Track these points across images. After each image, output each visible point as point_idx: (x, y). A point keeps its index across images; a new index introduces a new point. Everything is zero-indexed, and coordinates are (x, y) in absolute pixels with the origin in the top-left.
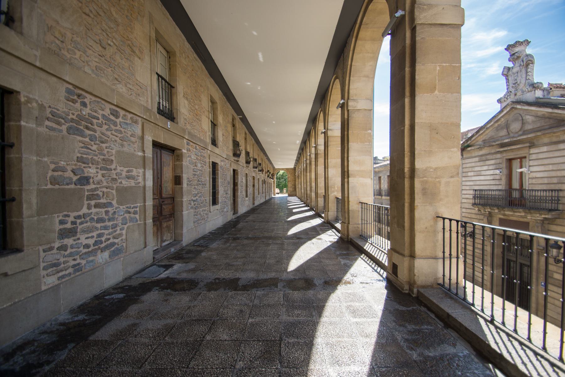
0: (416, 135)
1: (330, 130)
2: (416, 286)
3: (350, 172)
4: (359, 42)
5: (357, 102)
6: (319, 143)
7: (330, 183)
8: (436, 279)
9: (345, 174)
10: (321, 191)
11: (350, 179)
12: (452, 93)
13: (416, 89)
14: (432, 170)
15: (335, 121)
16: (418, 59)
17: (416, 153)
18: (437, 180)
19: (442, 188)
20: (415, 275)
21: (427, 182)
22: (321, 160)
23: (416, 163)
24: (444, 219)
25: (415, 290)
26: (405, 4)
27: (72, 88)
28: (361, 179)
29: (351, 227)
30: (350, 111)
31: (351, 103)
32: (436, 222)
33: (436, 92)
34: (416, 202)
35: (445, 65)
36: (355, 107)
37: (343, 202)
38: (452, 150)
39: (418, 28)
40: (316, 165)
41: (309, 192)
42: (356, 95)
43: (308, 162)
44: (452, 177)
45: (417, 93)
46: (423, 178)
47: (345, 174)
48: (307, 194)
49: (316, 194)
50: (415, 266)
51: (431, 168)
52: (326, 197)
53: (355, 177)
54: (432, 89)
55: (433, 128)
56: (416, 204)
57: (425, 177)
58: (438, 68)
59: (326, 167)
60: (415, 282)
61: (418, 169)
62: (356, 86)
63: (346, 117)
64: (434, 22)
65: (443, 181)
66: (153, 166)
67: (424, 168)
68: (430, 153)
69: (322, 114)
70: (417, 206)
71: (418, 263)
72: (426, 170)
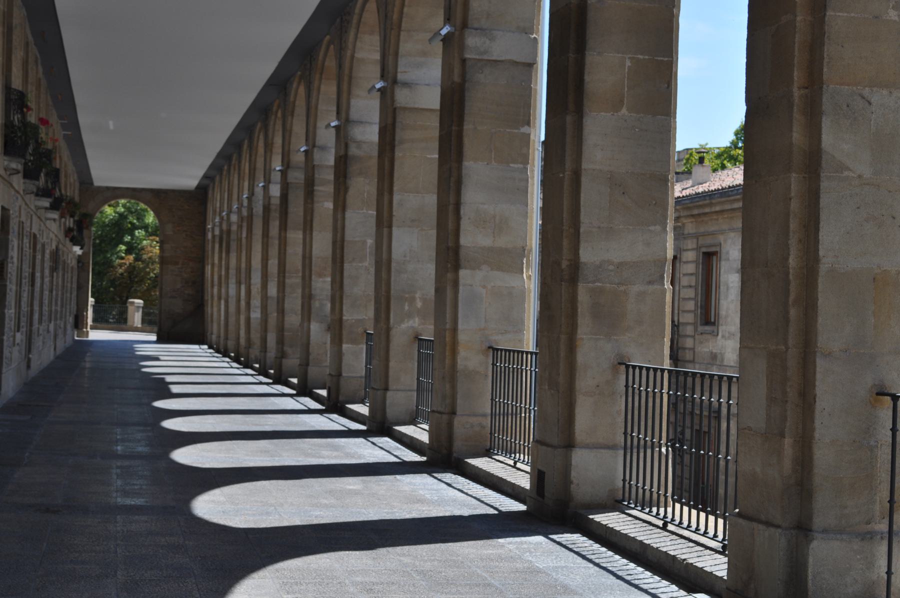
0: (582, 195)
1: (406, 84)
3: (462, 253)
5: (492, 39)
6: (354, 115)
7: (398, 283)
9: (450, 257)
10: (360, 314)
11: (462, 273)
13: (585, 101)
14: (611, 267)
15: (424, 54)
17: (582, 230)
18: (622, 288)
20: (571, 482)
22: (363, 186)
23: (581, 252)
24: (627, 367)
27: (448, 326)
29: (457, 421)
31: (472, 41)
33: (624, 111)
34: (579, 331)
35: (641, 57)
36: (485, 52)
38: (652, 228)
40: (341, 206)
41: (293, 320)
43: (297, 177)
44: (650, 283)
45: (586, 109)
46: (594, 282)
47: (450, 257)
48: (281, 329)
49: (337, 328)
50: (573, 462)
51: (610, 262)
52: (378, 343)
56: (579, 336)
58: (628, 63)
59: (384, 222)
61: (585, 264)
63: (385, 256)
67: (598, 263)
69: (302, 90)
70: (582, 339)
71: (579, 457)
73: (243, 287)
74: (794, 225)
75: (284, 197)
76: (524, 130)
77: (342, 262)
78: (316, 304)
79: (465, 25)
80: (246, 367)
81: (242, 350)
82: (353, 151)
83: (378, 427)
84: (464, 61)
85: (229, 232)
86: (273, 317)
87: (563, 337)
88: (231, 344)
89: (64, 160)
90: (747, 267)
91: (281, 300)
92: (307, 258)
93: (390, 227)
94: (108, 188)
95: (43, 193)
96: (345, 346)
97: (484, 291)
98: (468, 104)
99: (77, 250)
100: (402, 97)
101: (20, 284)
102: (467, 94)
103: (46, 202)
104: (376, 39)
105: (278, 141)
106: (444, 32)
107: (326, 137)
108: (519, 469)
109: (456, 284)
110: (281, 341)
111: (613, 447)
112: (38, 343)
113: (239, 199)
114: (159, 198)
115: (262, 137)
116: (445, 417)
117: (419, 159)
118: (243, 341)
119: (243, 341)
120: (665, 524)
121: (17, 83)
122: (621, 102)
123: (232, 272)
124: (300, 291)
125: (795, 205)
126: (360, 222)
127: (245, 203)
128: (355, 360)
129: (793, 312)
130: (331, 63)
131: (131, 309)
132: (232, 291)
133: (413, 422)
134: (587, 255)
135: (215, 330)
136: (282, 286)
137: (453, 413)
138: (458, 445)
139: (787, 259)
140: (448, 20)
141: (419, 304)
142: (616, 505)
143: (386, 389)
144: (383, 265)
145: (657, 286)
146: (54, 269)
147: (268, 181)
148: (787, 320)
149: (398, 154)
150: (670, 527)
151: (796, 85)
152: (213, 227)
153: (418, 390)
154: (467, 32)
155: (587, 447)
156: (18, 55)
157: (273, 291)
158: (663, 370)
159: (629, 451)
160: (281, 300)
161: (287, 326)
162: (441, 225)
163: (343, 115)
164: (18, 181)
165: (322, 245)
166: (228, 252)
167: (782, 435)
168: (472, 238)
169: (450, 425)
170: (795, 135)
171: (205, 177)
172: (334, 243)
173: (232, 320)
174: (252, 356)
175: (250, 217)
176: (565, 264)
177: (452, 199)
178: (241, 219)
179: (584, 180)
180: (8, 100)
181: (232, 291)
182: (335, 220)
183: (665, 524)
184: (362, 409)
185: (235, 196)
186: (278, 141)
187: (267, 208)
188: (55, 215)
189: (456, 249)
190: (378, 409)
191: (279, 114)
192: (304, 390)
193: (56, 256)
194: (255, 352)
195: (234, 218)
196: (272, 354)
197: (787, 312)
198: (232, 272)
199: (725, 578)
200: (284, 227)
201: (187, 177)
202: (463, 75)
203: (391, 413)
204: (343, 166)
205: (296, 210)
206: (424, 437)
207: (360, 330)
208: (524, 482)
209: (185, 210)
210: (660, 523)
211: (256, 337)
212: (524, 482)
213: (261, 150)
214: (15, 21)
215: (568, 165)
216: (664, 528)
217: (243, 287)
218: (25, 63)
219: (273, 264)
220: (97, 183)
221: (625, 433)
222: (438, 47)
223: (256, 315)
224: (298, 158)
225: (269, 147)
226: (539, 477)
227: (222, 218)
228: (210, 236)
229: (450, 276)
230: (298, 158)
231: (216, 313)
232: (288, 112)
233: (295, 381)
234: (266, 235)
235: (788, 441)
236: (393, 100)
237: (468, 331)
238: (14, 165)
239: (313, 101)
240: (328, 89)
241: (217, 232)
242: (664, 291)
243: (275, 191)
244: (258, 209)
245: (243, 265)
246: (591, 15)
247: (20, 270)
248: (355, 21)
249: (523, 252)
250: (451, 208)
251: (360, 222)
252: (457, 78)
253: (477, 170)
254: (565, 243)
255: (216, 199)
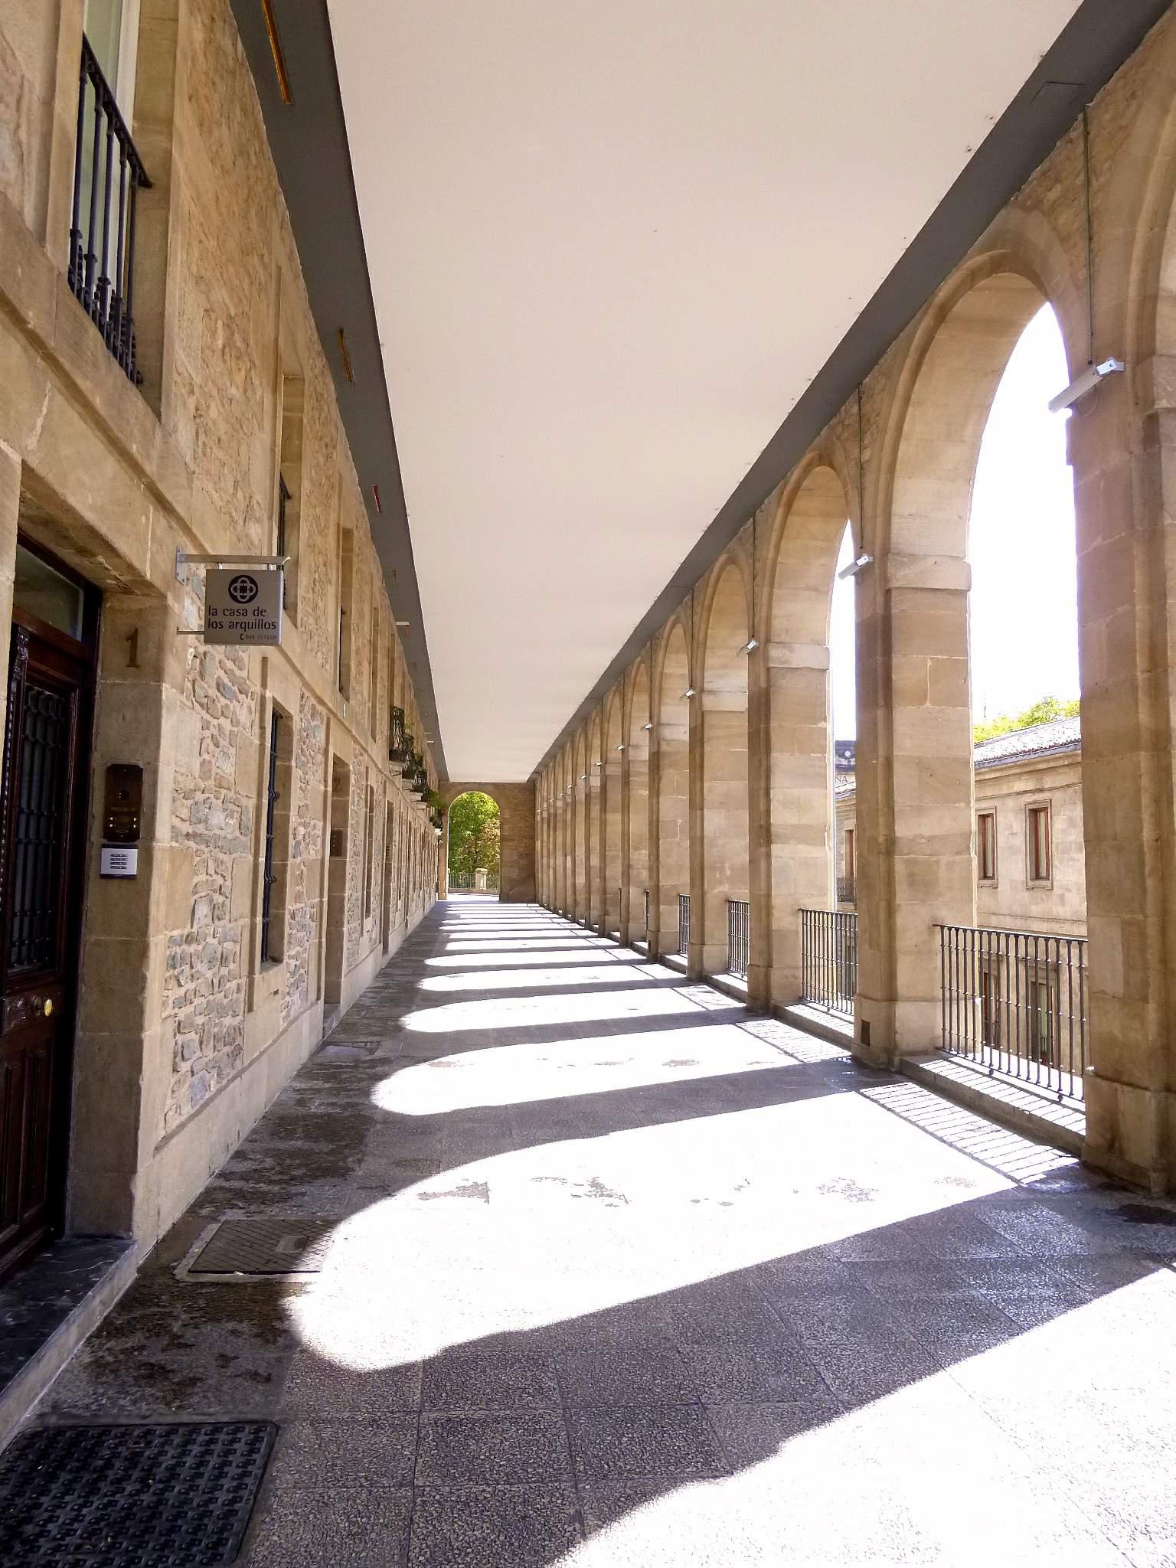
1: (711, 692)
2: (897, 1052)
3: (773, 829)
4: (793, 519)
6: (664, 719)
8: (934, 1039)
9: (762, 834)
11: (774, 847)
12: (955, 706)
16: (897, 646)
19: (942, 873)
21: (915, 862)
22: (676, 777)
24: (943, 927)
25: (897, 1060)
26: (873, 544)
28: (800, 847)
30: (772, 672)
31: (775, 653)
32: (931, 933)
33: (928, 704)
36: (787, 662)
37: (694, 904)
39: (894, 593)
40: (655, 792)
42: (787, 631)
43: (614, 770)
44: (958, 853)
45: (895, 704)
49: (654, 895)
53: (785, 841)
54: (922, 699)
55: (923, 766)
57: (912, 853)
58: (929, 663)
59: (697, 805)
60: (896, 1047)
62: (787, 610)
64: (921, 585)
65: (944, 859)
66: (769, 864)
68: (920, 810)
69: (617, 702)
72: (913, 840)
73: (569, 858)
74: (1146, 800)
75: (604, 787)
76: (821, 725)
77: (658, 839)
78: (633, 872)
79: (768, 641)
80: (602, 935)
81: (570, 908)
82: (664, 748)
83: (698, 977)
84: (768, 670)
85: (555, 815)
86: (596, 882)
87: (883, 903)
88: (559, 904)
89: (428, 763)
90: (1094, 840)
91: (603, 870)
92: (626, 836)
93: (702, 809)
94: (460, 783)
95: (416, 789)
96: (662, 907)
97: (792, 862)
98: (773, 705)
99: (438, 832)
100: (708, 702)
101: (400, 862)
102: (772, 697)
103: (418, 796)
104: (684, 659)
105: (597, 742)
106: (750, 646)
107: (640, 738)
108: (1064, 1106)
109: (768, 855)
110: (604, 902)
111: (932, 1000)
112: (412, 907)
113: (564, 790)
114: (499, 790)
115: (582, 740)
116: (763, 970)
117: (728, 752)
118: (569, 901)
119: (569, 901)
120: (991, 1072)
121: (397, 704)
122: (925, 698)
123: (559, 846)
124: (620, 861)
125: (1145, 782)
126: (674, 805)
127: (569, 792)
128: (671, 918)
129: (1150, 883)
130: (643, 679)
131: (477, 875)
132: (560, 861)
133: (678, 953)
134: (901, 830)
135: (545, 894)
136: (603, 857)
137: (769, 966)
138: (776, 996)
139: (1141, 831)
140: (753, 636)
141: (728, 873)
142: (726, 971)
143: (703, 944)
144: (698, 842)
145: (964, 857)
146: (423, 847)
147: (588, 774)
148: (1144, 891)
149: (707, 748)
150: (996, 1074)
151: (1139, 669)
152: (542, 811)
153: (730, 944)
154: (771, 646)
155: (909, 1000)
156: (398, 681)
157: (595, 861)
158: (973, 931)
159: (947, 1004)
160: (603, 870)
161: (608, 890)
162: (753, 808)
163: (655, 719)
164: (399, 781)
165: (639, 824)
166: (555, 831)
167: (1145, 1000)
168: (779, 817)
169: (767, 976)
170: (1141, 716)
171: (535, 772)
172: (651, 823)
173: (560, 884)
174: (578, 914)
175: (574, 803)
176: (881, 839)
177: (763, 784)
178: (566, 804)
179: (896, 766)
180: (392, 718)
181: (560, 861)
182: (651, 805)
183: (991, 1072)
184: (682, 960)
185: (560, 786)
186: (597, 742)
187: (588, 796)
188: (423, 806)
189: (767, 828)
190: (697, 960)
191: (597, 721)
192: (626, 943)
193: (424, 838)
194: (581, 909)
195: (559, 804)
196: (595, 913)
197: (1143, 882)
198: (559, 846)
199: (1083, 1133)
200: (604, 810)
201: (521, 774)
202: (768, 680)
203: (708, 964)
204: (656, 760)
205: (615, 796)
206: (743, 986)
207: (674, 894)
208: (1078, 1125)
209: (520, 798)
210: (986, 1071)
211: (581, 897)
212: (849, 1031)
213: (582, 750)
214: (396, 655)
215: (881, 752)
216: (990, 1075)
217: (569, 858)
218: (403, 687)
219: (595, 841)
220: (452, 780)
221: (943, 987)
222: (745, 661)
223: (581, 880)
224: (615, 755)
225: (588, 748)
226: (864, 1028)
227: (549, 805)
228: (539, 818)
229: (763, 850)
230: (615, 755)
231: (545, 879)
232: (605, 718)
233: (618, 934)
234: (588, 817)
235: (1152, 1007)
236: (701, 705)
237: (782, 899)
238: (397, 768)
239: (627, 709)
240: (640, 701)
241: (545, 815)
242: (970, 861)
243: (596, 782)
244: (581, 796)
245: (569, 841)
246: (895, 623)
247: (400, 850)
248: (663, 643)
249: (824, 828)
250: (762, 792)
251: (674, 805)
252: (763, 685)
253: (782, 760)
254: (881, 821)
255: (544, 789)
